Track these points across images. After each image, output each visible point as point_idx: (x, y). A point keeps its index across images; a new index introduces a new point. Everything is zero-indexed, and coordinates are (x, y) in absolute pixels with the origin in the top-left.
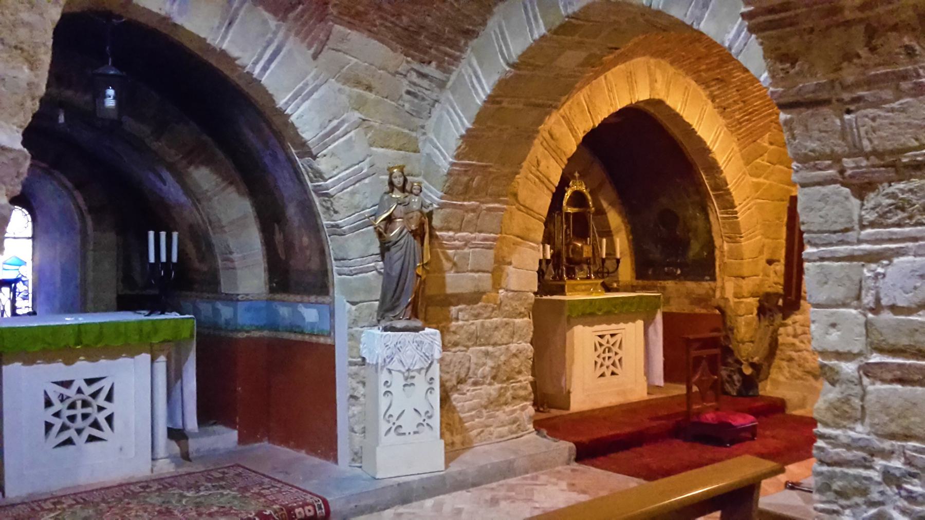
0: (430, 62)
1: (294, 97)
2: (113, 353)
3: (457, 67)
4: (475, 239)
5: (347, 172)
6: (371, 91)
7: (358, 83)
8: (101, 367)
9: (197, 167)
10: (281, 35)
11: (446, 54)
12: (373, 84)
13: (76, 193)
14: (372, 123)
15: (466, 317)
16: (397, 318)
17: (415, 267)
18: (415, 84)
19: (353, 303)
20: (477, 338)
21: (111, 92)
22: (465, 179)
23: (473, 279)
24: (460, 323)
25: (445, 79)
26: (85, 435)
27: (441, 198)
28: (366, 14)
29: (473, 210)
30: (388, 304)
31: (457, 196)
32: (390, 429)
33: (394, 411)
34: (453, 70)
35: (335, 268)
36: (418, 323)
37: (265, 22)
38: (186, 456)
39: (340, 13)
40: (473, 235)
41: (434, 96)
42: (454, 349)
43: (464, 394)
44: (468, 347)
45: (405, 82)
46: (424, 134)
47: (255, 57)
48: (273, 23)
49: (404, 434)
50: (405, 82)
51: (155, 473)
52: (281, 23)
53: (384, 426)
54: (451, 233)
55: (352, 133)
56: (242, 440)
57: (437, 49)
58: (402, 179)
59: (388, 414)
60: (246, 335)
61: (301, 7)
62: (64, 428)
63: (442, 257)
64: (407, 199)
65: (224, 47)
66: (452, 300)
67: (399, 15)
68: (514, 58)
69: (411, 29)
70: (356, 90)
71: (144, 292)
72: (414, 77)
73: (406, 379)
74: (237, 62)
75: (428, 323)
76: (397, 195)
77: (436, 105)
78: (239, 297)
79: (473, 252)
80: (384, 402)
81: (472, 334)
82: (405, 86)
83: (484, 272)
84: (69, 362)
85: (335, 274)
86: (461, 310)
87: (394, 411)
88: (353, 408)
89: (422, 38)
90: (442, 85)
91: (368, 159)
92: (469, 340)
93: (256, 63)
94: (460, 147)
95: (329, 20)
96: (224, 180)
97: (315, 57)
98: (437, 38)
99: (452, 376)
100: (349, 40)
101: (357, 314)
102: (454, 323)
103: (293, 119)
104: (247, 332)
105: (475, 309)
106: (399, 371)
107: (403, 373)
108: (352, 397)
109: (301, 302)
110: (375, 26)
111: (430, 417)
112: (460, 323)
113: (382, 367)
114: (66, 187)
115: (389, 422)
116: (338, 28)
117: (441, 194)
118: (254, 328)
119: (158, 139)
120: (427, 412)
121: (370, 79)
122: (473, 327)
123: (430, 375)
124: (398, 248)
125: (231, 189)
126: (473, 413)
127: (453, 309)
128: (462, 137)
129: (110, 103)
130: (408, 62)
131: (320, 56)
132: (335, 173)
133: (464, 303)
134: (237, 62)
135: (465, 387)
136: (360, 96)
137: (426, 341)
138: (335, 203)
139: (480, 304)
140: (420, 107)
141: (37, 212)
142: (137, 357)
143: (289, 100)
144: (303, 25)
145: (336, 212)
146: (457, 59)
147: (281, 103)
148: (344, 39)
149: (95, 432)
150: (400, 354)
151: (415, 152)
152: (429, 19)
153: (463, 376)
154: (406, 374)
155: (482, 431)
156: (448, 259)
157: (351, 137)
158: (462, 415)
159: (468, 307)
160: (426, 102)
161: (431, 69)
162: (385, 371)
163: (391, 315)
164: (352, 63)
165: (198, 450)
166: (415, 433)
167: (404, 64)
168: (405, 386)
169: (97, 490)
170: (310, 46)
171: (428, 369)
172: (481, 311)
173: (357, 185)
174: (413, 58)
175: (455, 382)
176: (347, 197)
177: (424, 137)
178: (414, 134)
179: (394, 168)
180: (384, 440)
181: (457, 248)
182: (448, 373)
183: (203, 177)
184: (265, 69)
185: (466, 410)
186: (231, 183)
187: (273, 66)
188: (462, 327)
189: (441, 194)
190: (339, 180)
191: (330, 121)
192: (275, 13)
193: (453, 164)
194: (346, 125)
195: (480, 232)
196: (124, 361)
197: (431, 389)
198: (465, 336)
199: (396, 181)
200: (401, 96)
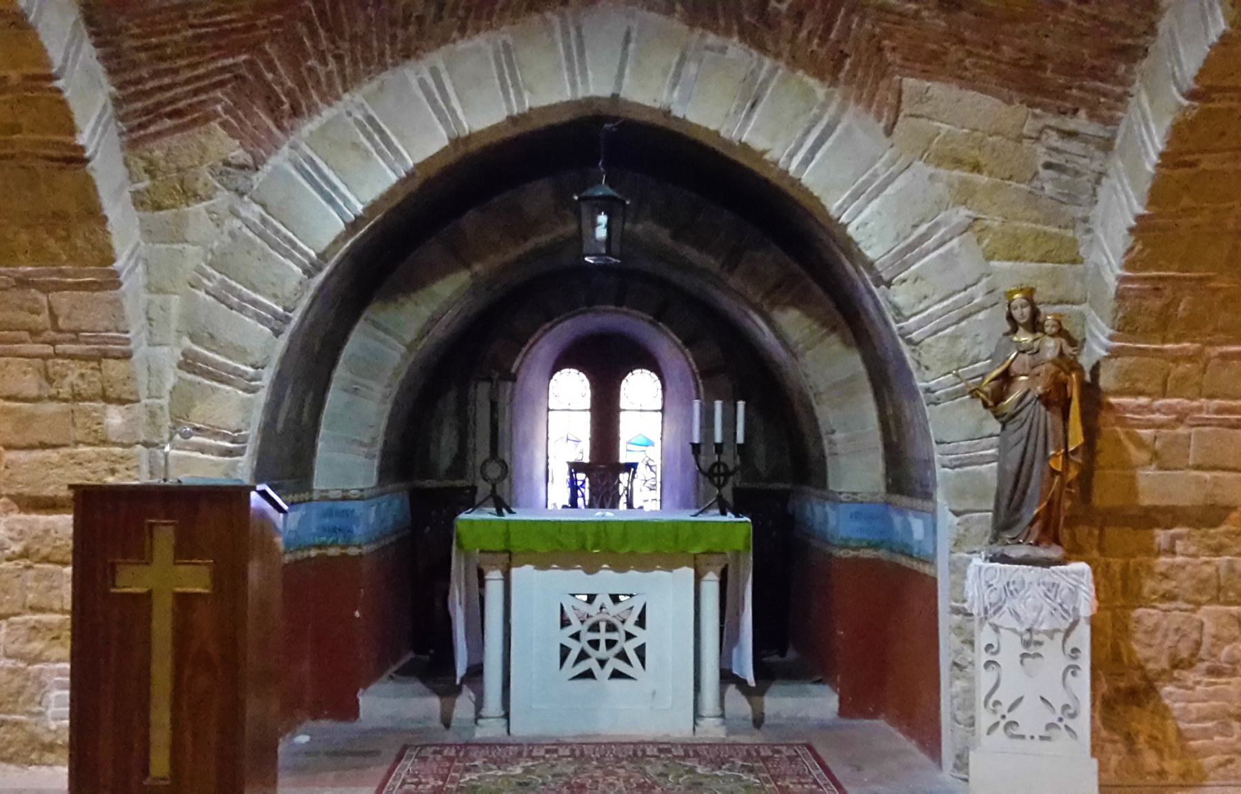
0: (1075, 111)
1: (855, 196)
2: (645, 565)
3: (1125, 112)
4: (1200, 409)
5: (945, 303)
6: (980, 172)
7: (958, 163)
8: (631, 580)
9: (782, 310)
10: (832, 109)
11: (1096, 91)
12: (983, 161)
13: (687, 351)
14: (988, 222)
15: (1193, 549)
16: (1015, 541)
17: (1046, 458)
18: (1056, 150)
19: (957, 514)
20: (1219, 589)
21: (602, 219)
22: (1157, 304)
23: (1200, 482)
24: (1179, 559)
25: (1108, 135)
26: (609, 669)
27: (1111, 338)
28: (945, 54)
29: (1190, 358)
30: (1002, 519)
31: (1146, 335)
32: (997, 724)
33: (1005, 696)
34: (1120, 119)
35: (937, 456)
36: (1055, 552)
37: (811, 91)
38: (758, 721)
39: (906, 59)
40: (1195, 404)
41: (1095, 166)
42: (1166, 606)
43: (1191, 688)
44: (1199, 604)
45: (1040, 150)
46: (1089, 231)
47: (792, 146)
48: (821, 91)
49: (1023, 737)
50: (1040, 150)
51: (698, 735)
52: (831, 89)
53: (985, 719)
54: (1143, 400)
55: (955, 241)
56: (843, 712)
57: (1081, 88)
58: (1027, 310)
59: (994, 698)
60: (852, 553)
61: (848, 62)
62: (583, 656)
63: (1126, 442)
64: (1036, 344)
65: (411, 163)
66: (1160, 517)
67: (997, 49)
68: (1190, 84)
69: (1022, 62)
70: (956, 173)
71: (770, 486)
72: (1054, 140)
73: (1027, 644)
74: (767, 157)
75: (1074, 552)
76: (1024, 338)
77: (1104, 180)
78: (842, 497)
79: (1197, 433)
80: (985, 680)
81: (1205, 581)
82: (1042, 155)
83: (1224, 469)
84: (591, 569)
85: (937, 466)
86: (1180, 537)
87: (1005, 696)
88: (957, 683)
89: (1048, 74)
90: (1107, 146)
91: (984, 280)
92: (1199, 591)
93: (791, 156)
94: (1132, 249)
95: (893, 73)
96: (823, 325)
97: (889, 131)
98: (1073, 68)
99: (1160, 652)
100: (929, 99)
101: (962, 531)
102: (1163, 559)
103: (851, 230)
104: (854, 549)
105: (1213, 537)
106: (1014, 630)
107: (1021, 635)
108: (955, 664)
109: (912, 509)
110: (966, 69)
111: (1073, 716)
112: (1179, 559)
113: (981, 622)
114: (676, 343)
115: (994, 712)
116: (910, 83)
117: (1109, 331)
118: (864, 544)
119: (731, 271)
120: (1066, 707)
121: (976, 153)
122: (1209, 569)
123: (1072, 642)
124: (1018, 424)
125: (833, 338)
126: (1209, 724)
127: (1161, 536)
128: (1131, 230)
129: (601, 233)
130: (1035, 116)
131: (896, 130)
132: (922, 306)
133: (1189, 525)
134: (767, 157)
135: (1190, 677)
136: (963, 182)
137: (1063, 584)
138: (923, 355)
139: (1223, 528)
140: (1080, 189)
141: (666, 377)
142: (677, 571)
143: (844, 202)
144: (861, 86)
145: (927, 368)
146: (1121, 99)
147: (833, 207)
148: (922, 98)
149: (622, 666)
150: (1014, 601)
151: (1074, 262)
152: (1049, 42)
153: (1185, 654)
154: (1027, 637)
155: (1230, 761)
156: (1140, 444)
157: (952, 249)
158: (1183, 725)
159: (1195, 532)
160: (1085, 178)
161: (1081, 123)
162: (987, 627)
163: (1007, 536)
164: (943, 133)
165: (777, 716)
166: (1042, 738)
167: (1030, 121)
168: (1024, 655)
169: (615, 744)
170: (879, 117)
171: (1068, 633)
172: (1226, 541)
173: (964, 323)
174: (1045, 108)
175: (1164, 663)
176: (943, 344)
177: (1088, 237)
178: (1070, 233)
179: (1011, 293)
180: (985, 740)
181: (1161, 426)
182: (1150, 646)
183: (793, 321)
184: (806, 162)
185: (1194, 716)
186: (834, 329)
187: (818, 156)
188: (1182, 567)
189: (1109, 331)
190: (930, 319)
191: (915, 226)
192: (819, 74)
193: (1123, 279)
194: (943, 230)
195: (1211, 397)
196: (659, 575)
197: (1074, 670)
198: (1187, 584)
199: (1016, 314)
200: (1036, 173)
